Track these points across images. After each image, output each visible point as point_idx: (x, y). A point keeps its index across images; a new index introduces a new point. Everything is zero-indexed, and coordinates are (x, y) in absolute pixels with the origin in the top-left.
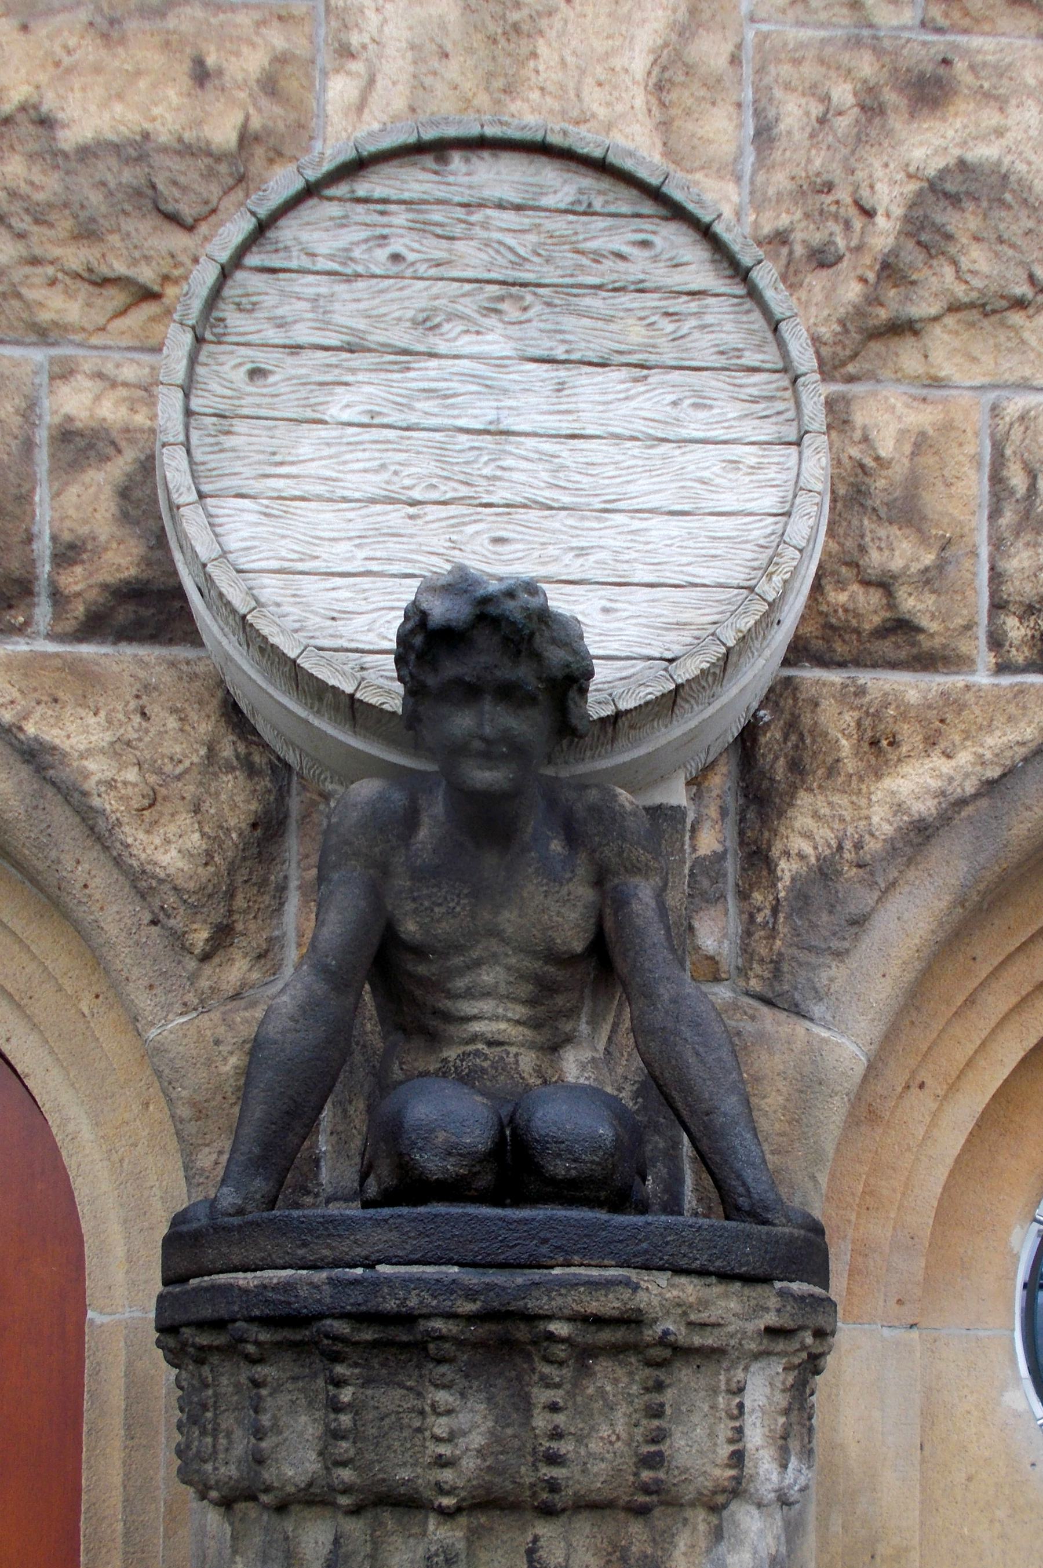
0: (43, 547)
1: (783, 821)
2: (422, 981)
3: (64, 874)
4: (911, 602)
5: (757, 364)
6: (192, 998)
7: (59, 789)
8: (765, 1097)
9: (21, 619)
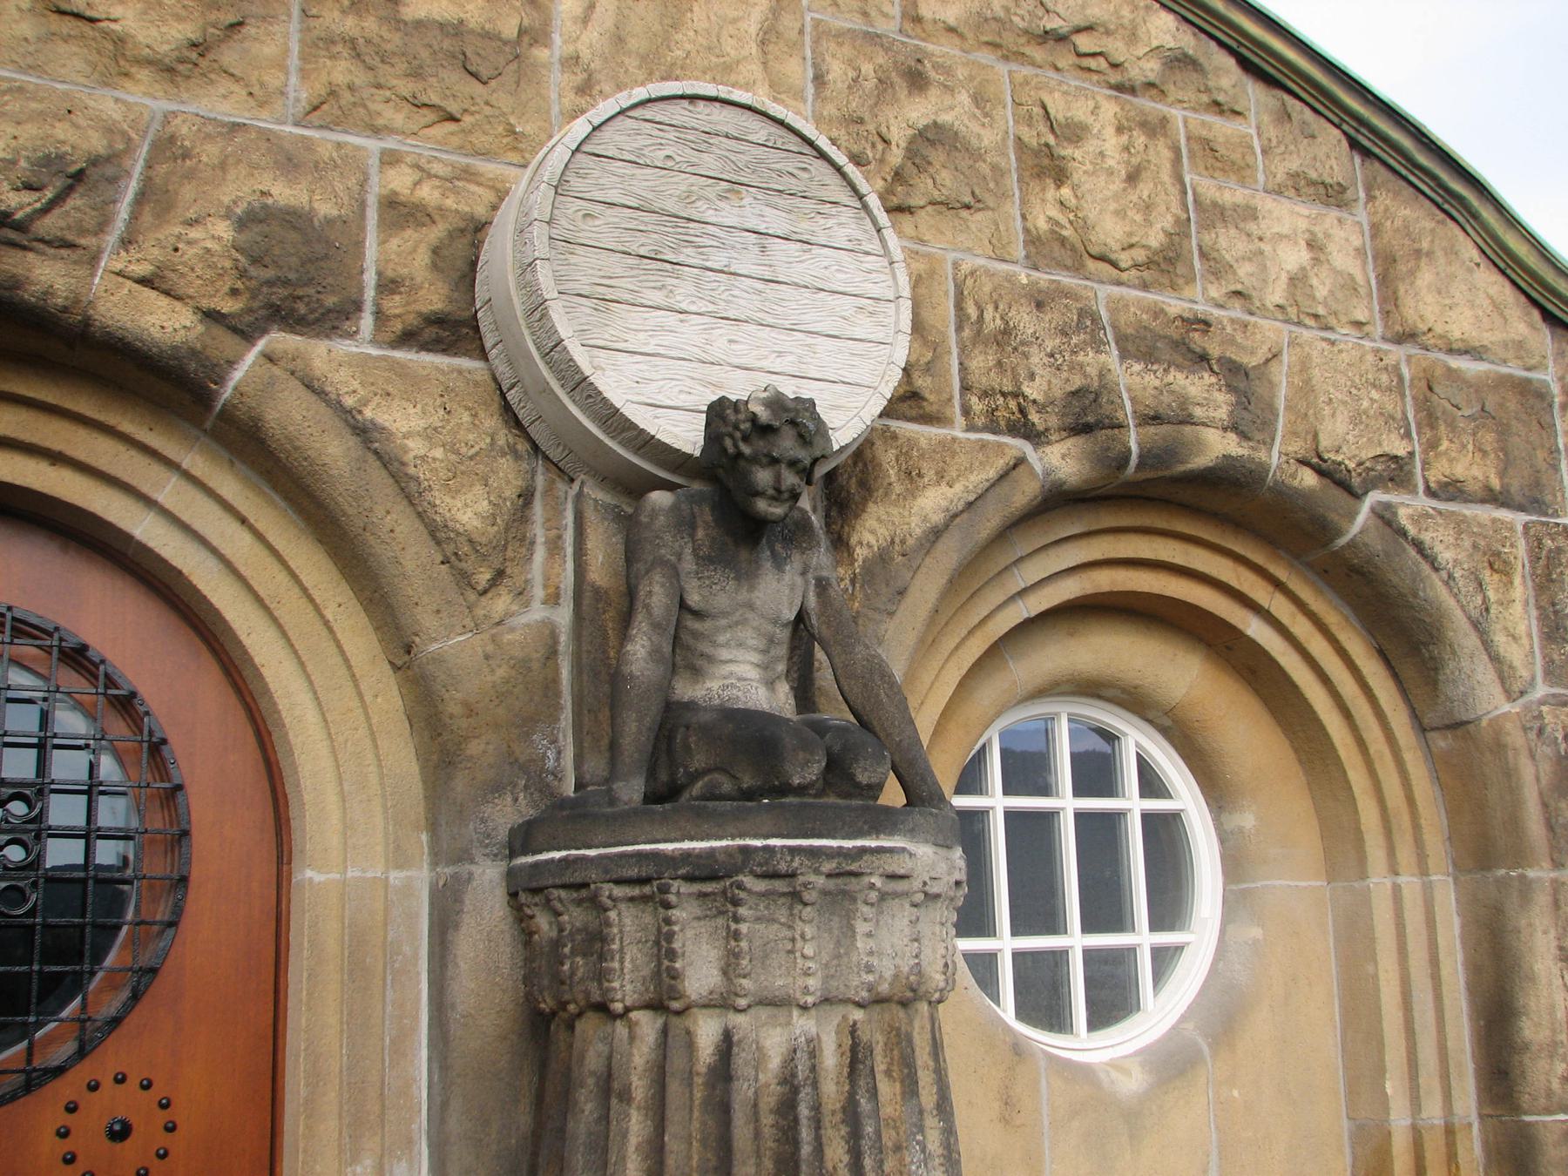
0: (370, 278)
2: (696, 635)
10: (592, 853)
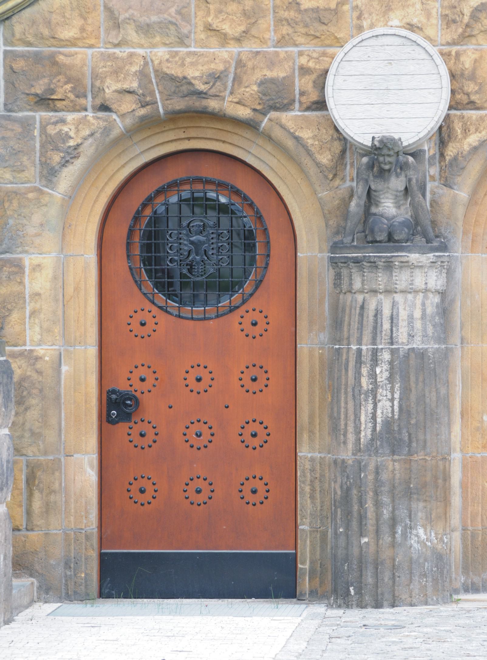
0: (297, 92)
2: (375, 196)
6: (328, 188)
10: (337, 255)
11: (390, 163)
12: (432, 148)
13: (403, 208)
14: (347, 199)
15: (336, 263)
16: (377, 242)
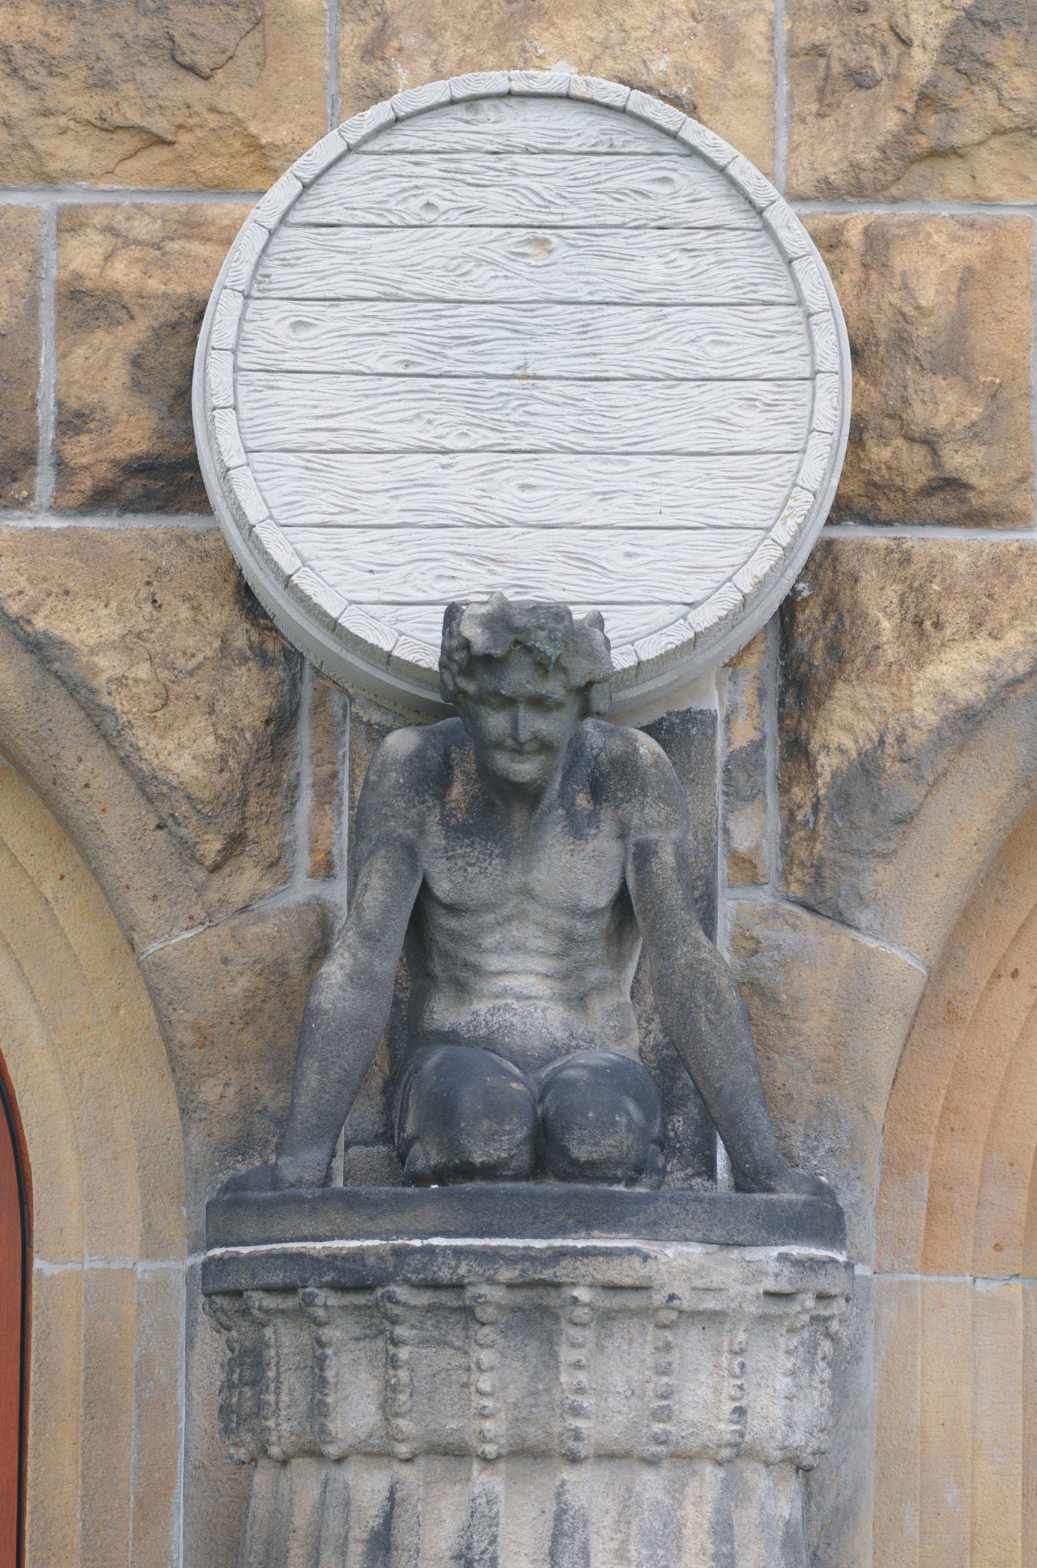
0: (46, 414)
1: (821, 713)
2: (455, 937)
3: (64, 770)
4: (958, 459)
5: (772, 298)
7: (64, 683)
8: (805, 1021)
9: (25, 493)
10: (245, 1250)
11: (545, 747)
12: (743, 713)
13: (600, 1006)
14: (296, 970)
15: (237, 1294)
16: (468, 1171)
